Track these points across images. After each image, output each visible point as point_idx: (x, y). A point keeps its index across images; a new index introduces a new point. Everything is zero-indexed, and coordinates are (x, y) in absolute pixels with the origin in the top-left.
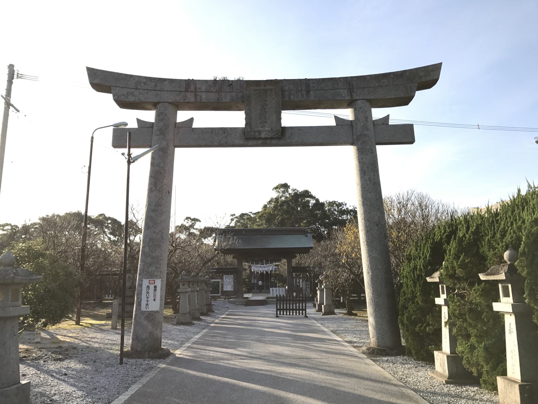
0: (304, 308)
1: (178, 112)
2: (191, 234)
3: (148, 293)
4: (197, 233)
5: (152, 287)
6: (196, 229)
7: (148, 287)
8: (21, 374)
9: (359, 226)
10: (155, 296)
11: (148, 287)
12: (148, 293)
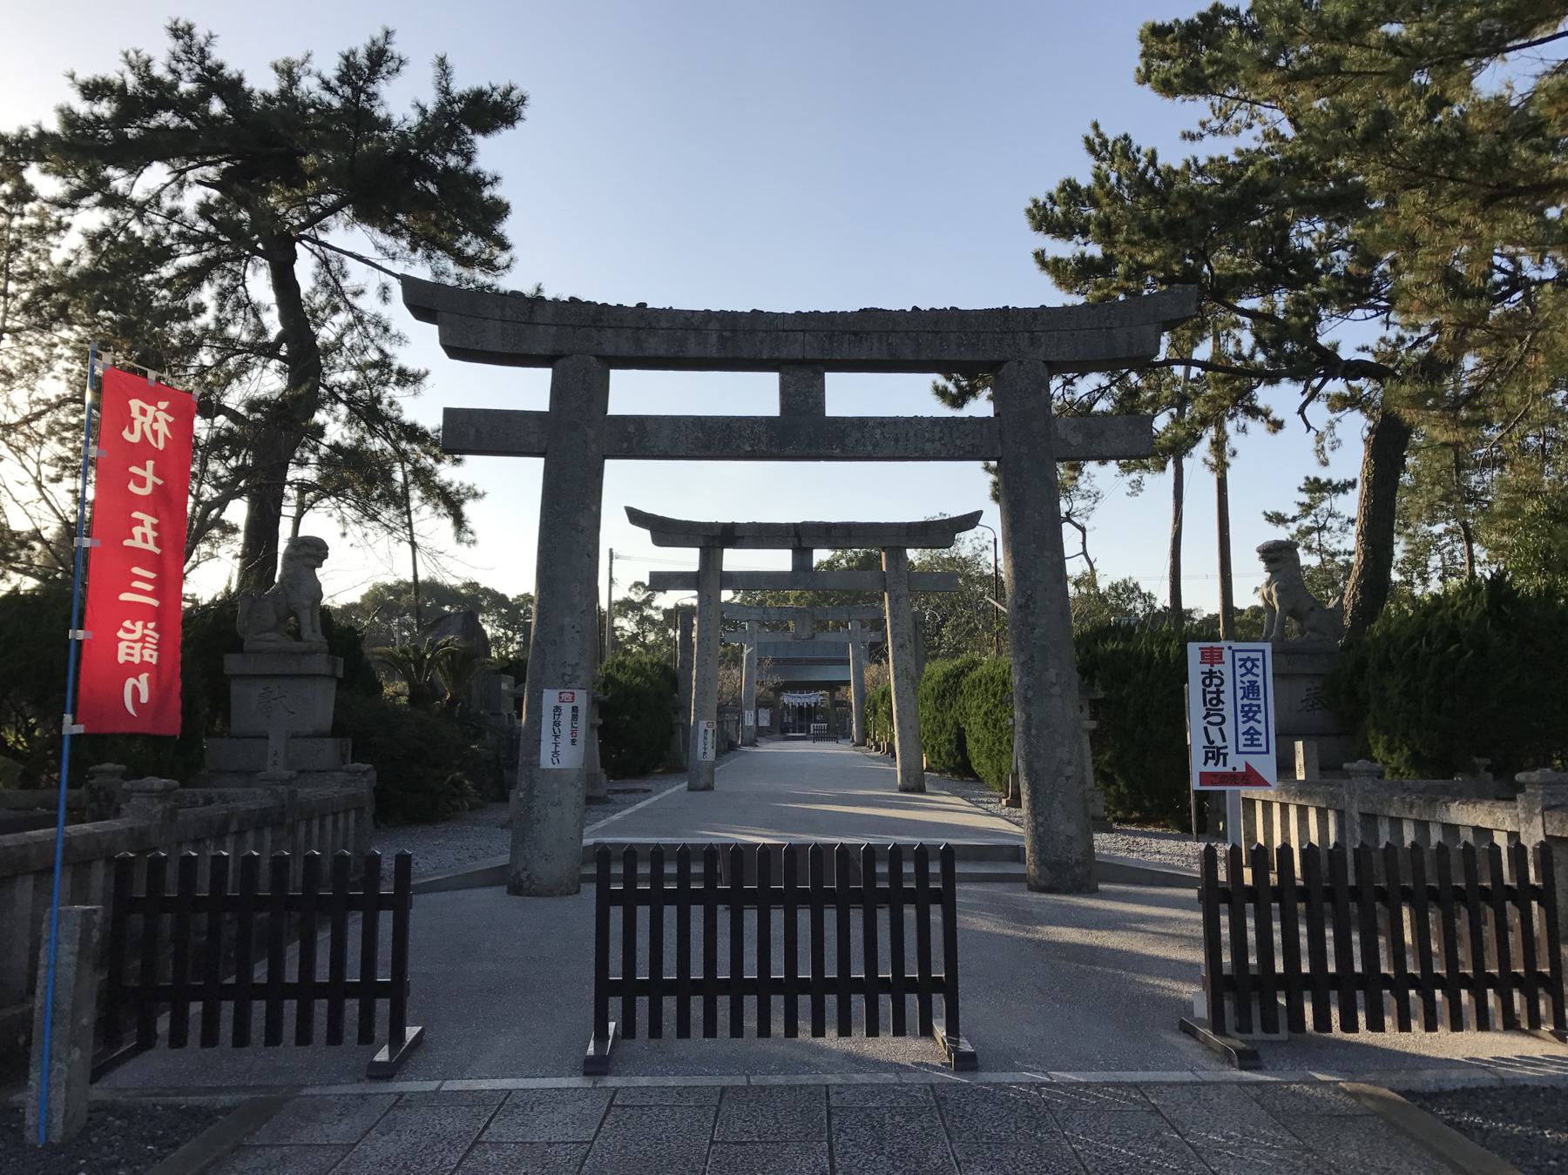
0: (939, 973)
1: (612, 372)
2: (644, 620)
3: (557, 724)
4: (659, 617)
5: (567, 709)
6: (657, 608)
7: (557, 708)
8: (240, 537)
9: (1145, 1079)
10: (574, 732)
11: (557, 708)
12: (557, 724)
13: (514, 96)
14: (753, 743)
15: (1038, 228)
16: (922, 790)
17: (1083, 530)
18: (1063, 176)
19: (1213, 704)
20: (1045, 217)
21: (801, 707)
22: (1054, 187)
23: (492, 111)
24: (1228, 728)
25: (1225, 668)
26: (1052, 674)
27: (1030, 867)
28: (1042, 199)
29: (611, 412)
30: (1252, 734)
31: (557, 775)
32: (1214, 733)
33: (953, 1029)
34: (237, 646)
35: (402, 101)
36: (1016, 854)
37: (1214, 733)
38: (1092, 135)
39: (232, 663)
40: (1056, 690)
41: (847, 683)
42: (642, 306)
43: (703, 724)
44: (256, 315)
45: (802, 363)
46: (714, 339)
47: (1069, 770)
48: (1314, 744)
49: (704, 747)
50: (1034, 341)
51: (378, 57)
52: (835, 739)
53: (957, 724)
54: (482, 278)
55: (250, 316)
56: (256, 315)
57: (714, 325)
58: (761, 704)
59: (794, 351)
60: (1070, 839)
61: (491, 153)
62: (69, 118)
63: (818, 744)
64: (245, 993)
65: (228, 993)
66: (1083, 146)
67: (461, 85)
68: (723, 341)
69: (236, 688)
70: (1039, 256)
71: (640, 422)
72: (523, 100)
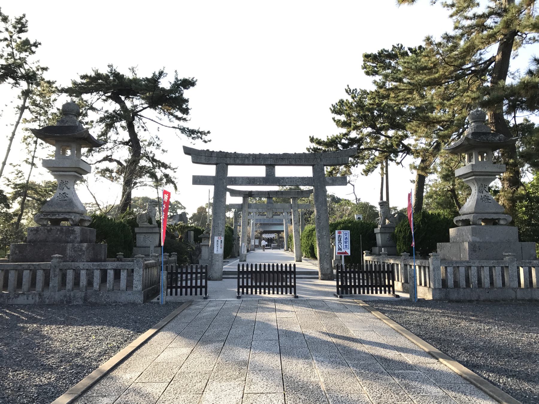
5: (220, 241)
13: (194, 80)
14: (254, 250)
15: (333, 112)
16: (301, 261)
17: (354, 186)
18: (340, 98)
19: (340, 241)
20: (334, 110)
21: (268, 239)
22: (337, 101)
23: (188, 83)
24: (342, 245)
25: (342, 235)
26: (324, 233)
27: (320, 275)
28: (334, 104)
29: (228, 176)
30: (346, 246)
31: (218, 255)
32: (340, 245)
33: (295, 293)
34: (137, 226)
35: (165, 84)
36: (317, 273)
37: (340, 245)
38: (347, 88)
39: (137, 230)
40: (325, 237)
41: (283, 231)
42: (235, 153)
43: (243, 244)
44: (116, 129)
45: (271, 165)
46: (251, 160)
47: (328, 254)
48: (386, 249)
49: (244, 251)
50: (321, 160)
51: (161, 73)
52: (279, 249)
53: (312, 244)
54: (317, 310)
55: (115, 130)
56: (116, 129)
57: (251, 157)
58: (256, 238)
59: (269, 163)
60: (328, 269)
61: (187, 94)
62: (75, 83)
63: (274, 250)
64: (181, 287)
65: (174, 287)
66: (345, 91)
67: (180, 77)
68: (253, 160)
69: (137, 236)
70: (334, 119)
71: (235, 178)
72: (197, 80)
